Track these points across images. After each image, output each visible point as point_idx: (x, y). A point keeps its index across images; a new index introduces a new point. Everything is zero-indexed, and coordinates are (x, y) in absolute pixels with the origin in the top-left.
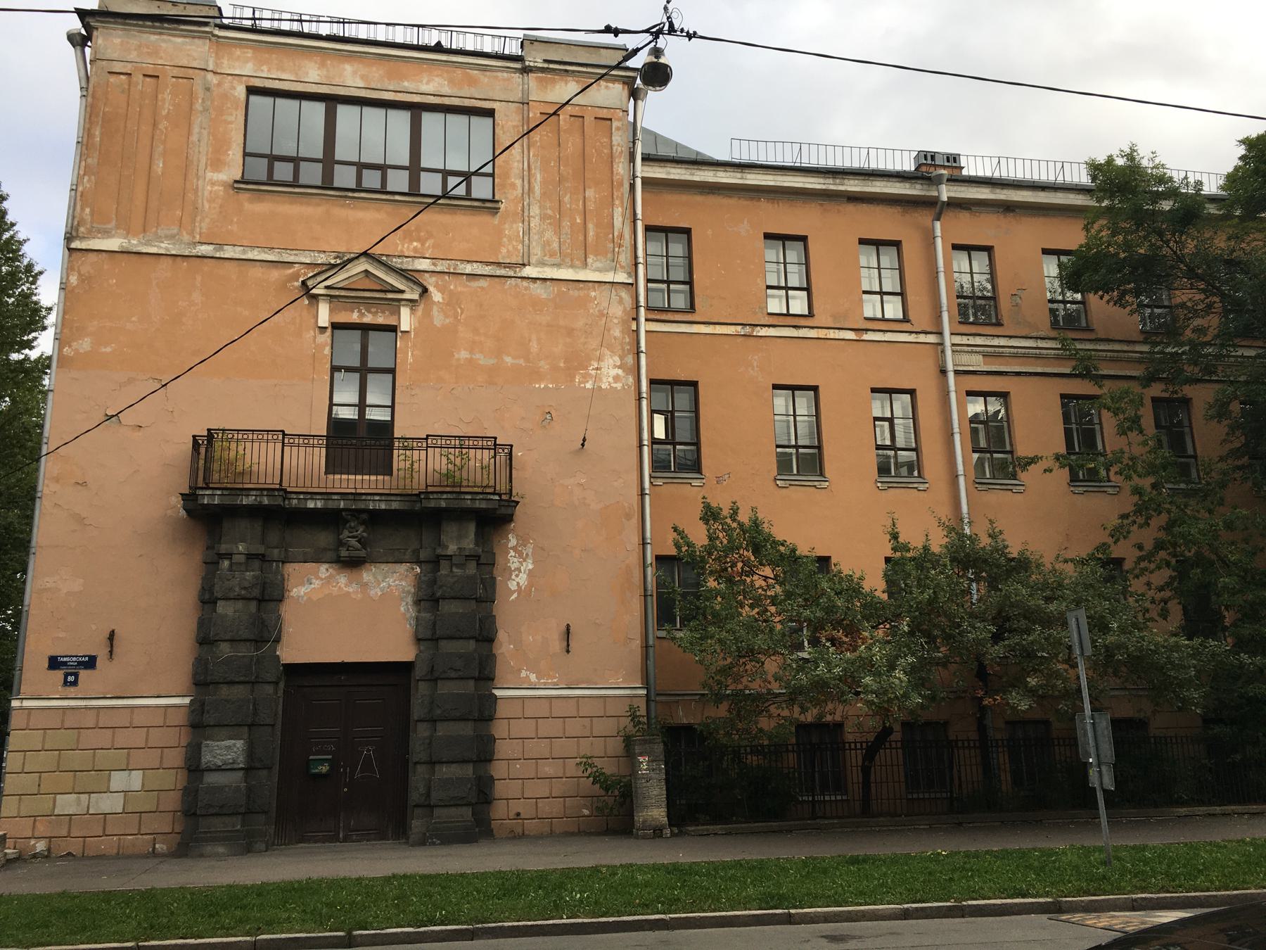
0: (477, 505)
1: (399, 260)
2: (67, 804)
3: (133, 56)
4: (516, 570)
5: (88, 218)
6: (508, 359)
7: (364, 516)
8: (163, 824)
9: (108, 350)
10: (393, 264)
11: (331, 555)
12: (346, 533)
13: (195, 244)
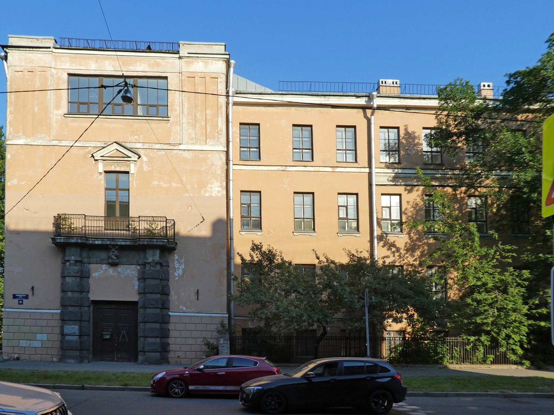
0: (159, 243)
1: (129, 144)
2: (23, 343)
3: (23, 64)
4: (178, 268)
5: (12, 131)
6: (174, 185)
7: (117, 247)
8: (55, 352)
9: (23, 183)
10: (127, 146)
11: (106, 261)
12: (111, 253)
13: (51, 141)
